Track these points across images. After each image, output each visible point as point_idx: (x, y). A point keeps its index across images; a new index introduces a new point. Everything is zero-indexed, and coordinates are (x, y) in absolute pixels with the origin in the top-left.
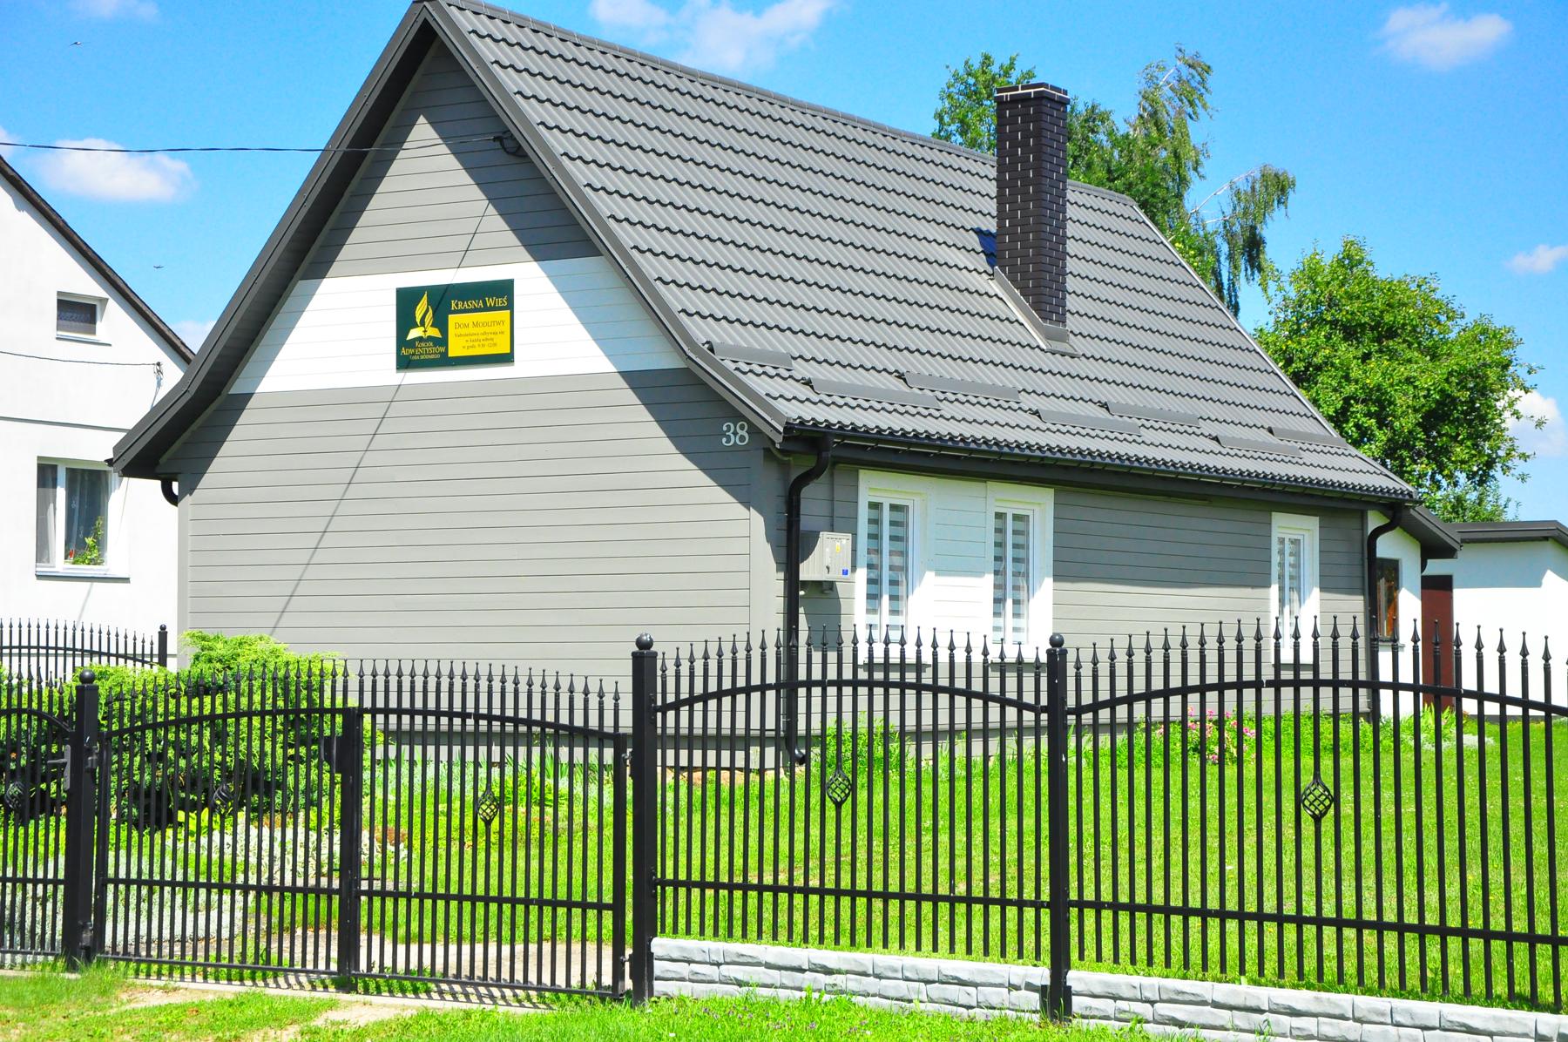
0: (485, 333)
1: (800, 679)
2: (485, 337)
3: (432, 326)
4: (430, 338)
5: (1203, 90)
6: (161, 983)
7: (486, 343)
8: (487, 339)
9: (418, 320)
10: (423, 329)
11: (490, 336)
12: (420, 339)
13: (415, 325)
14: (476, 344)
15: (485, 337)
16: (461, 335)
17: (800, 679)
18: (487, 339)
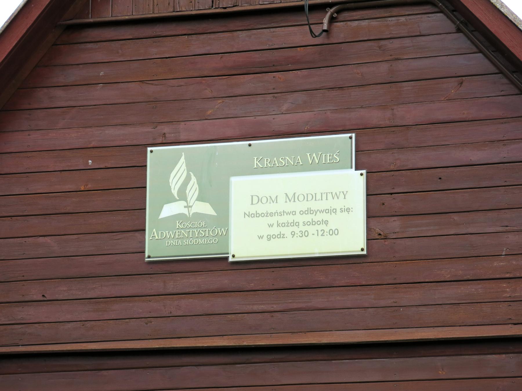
0: (309, 211)
1: (354, 134)
2: (308, 218)
3: (198, 199)
4: (198, 216)
5: (274, 215)
6: (268, 98)
7: (312, 229)
8: (313, 223)
9: (175, 192)
10: (184, 203)
11: (319, 217)
12: (180, 217)
13: (171, 199)
14: (287, 231)
15: (308, 218)
16: (257, 215)
17: (354, 134)
18: (313, 223)
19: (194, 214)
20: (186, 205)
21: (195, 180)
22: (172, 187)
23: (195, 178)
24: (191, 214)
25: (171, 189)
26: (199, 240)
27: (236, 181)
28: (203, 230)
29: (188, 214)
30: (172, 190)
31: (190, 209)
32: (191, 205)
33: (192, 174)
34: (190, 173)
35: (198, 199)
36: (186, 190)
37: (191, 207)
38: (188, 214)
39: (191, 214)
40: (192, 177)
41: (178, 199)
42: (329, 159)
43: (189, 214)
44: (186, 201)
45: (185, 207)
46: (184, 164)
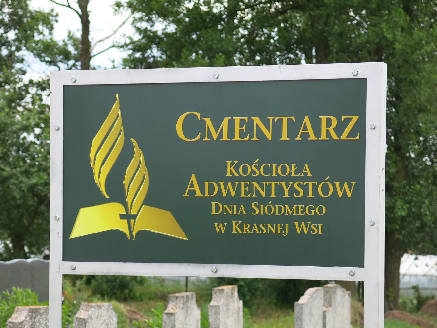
3: (148, 201)
10: (119, 208)
19: (140, 233)
20: (124, 212)
21: (141, 158)
22: (96, 171)
23: (141, 152)
24: (134, 234)
25: (93, 174)
26: (285, 208)
27: (383, 66)
28: (301, 183)
29: (128, 233)
30: (96, 177)
31: (132, 221)
32: (133, 212)
33: (135, 143)
34: (131, 141)
35: (148, 201)
36: (123, 179)
37: (134, 217)
38: (128, 233)
39: (134, 234)
40: (135, 149)
41: (107, 197)
42: (280, 229)
43: (131, 232)
44: (125, 204)
45: (122, 217)
46: (119, 121)
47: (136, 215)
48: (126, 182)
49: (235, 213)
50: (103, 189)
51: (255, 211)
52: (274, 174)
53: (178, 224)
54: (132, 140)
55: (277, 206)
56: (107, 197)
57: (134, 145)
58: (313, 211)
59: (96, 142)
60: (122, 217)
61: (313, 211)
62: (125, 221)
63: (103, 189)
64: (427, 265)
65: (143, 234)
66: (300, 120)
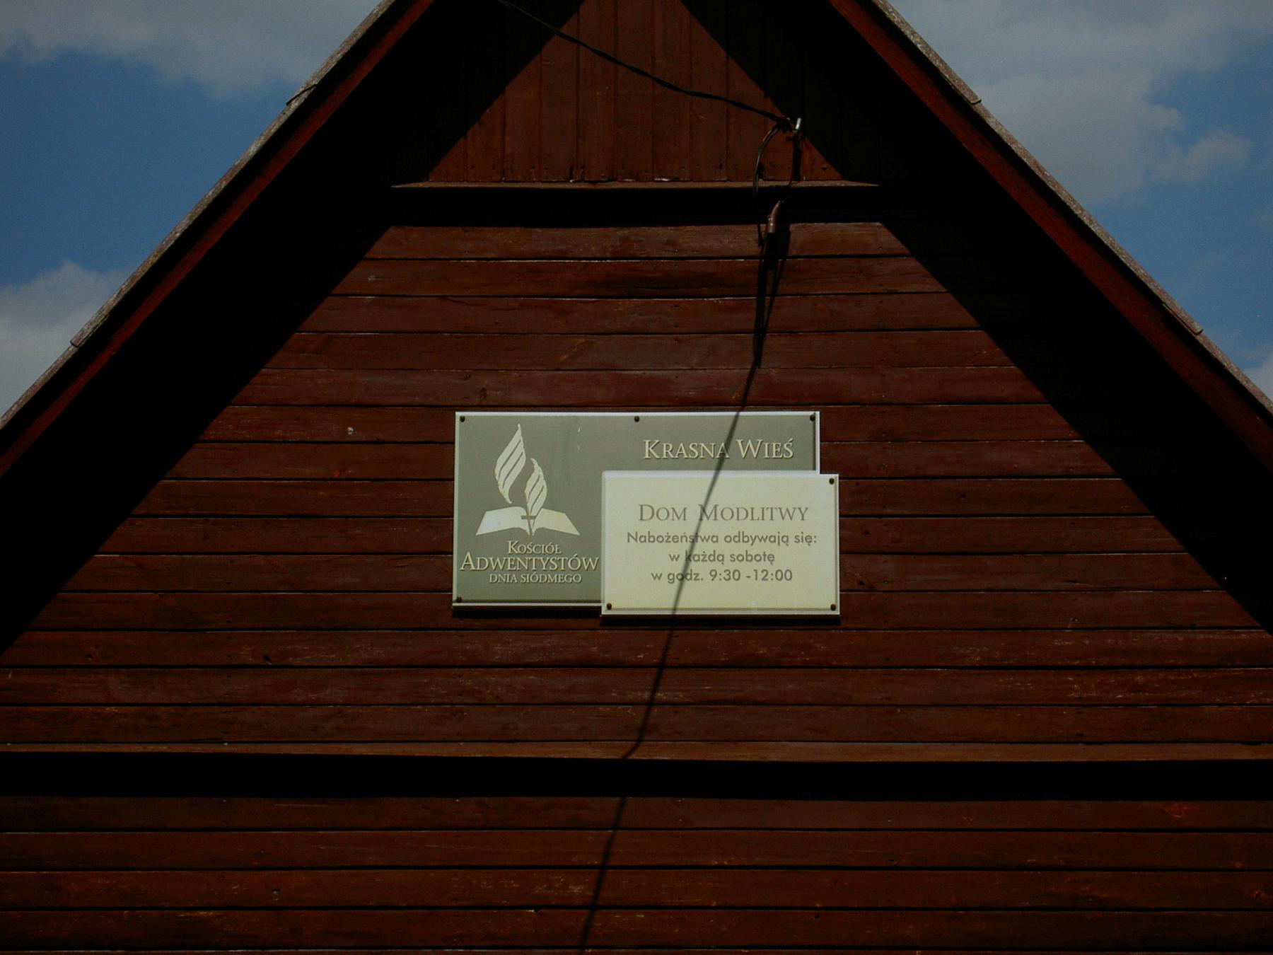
10: (522, 511)
20: (525, 514)
22: (500, 483)
24: (533, 531)
26: (548, 577)
29: (528, 531)
30: (500, 487)
31: (532, 521)
32: (533, 514)
37: (534, 518)
38: (528, 531)
39: (533, 531)
41: (510, 503)
43: (531, 530)
44: (526, 509)
45: (523, 517)
47: (535, 517)
48: (527, 491)
49: (508, 581)
50: (506, 496)
51: (523, 580)
52: (543, 552)
53: (569, 520)
54: (532, 459)
55: (541, 575)
56: (510, 503)
57: (756, 288)
58: (571, 579)
59: (501, 461)
60: (523, 517)
61: (571, 579)
62: (526, 521)
63: (506, 496)
64: (749, 577)
65: (542, 531)
66: (496, 559)
